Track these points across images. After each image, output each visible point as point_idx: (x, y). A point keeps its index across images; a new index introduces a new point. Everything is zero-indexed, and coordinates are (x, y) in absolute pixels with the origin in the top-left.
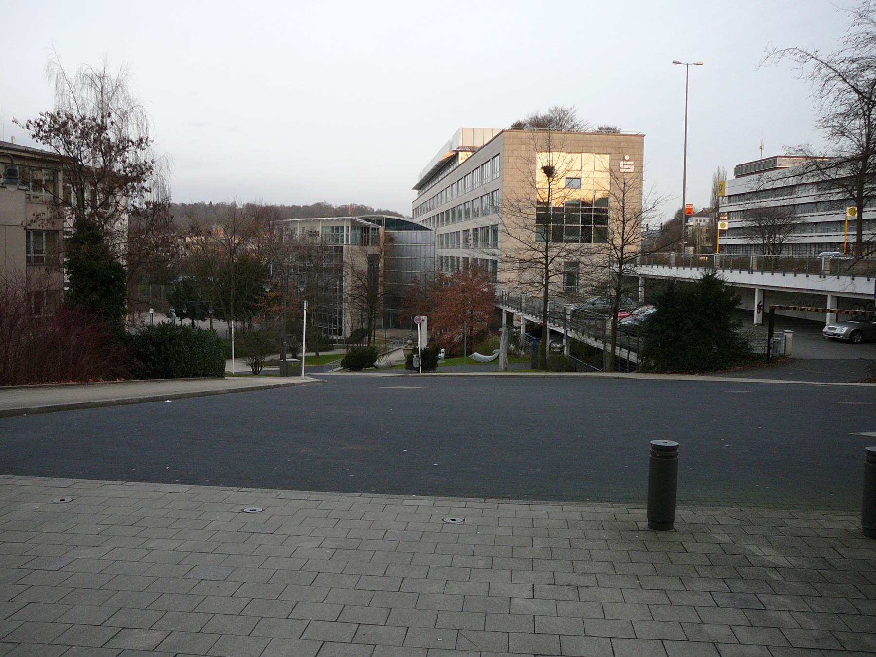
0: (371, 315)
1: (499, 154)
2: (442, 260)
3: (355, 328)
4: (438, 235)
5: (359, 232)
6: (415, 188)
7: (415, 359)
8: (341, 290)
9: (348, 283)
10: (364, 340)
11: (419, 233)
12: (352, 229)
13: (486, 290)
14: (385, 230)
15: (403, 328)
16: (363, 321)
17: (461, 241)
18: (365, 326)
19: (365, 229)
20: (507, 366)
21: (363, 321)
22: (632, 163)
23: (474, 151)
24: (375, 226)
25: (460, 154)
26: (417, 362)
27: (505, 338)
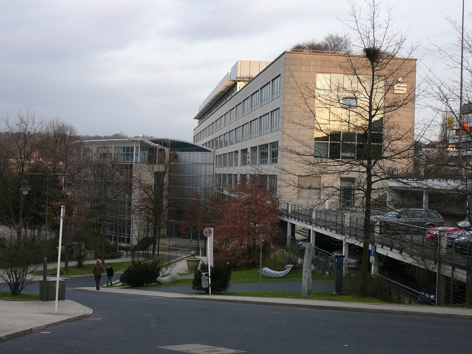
0: (156, 226)
1: (280, 75)
2: (220, 177)
3: (142, 237)
4: (216, 156)
5: (147, 153)
6: (196, 118)
7: (204, 278)
8: (130, 204)
9: (137, 194)
10: (149, 248)
11: (200, 154)
12: (141, 150)
13: (269, 202)
14: (170, 151)
15: (184, 238)
16: (148, 230)
17: (239, 160)
18: (150, 235)
19: (152, 150)
20: (311, 288)
21: (148, 230)
22: (405, 85)
23: (250, 80)
24: (161, 147)
25: (238, 83)
26: (207, 282)
27: (309, 255)
